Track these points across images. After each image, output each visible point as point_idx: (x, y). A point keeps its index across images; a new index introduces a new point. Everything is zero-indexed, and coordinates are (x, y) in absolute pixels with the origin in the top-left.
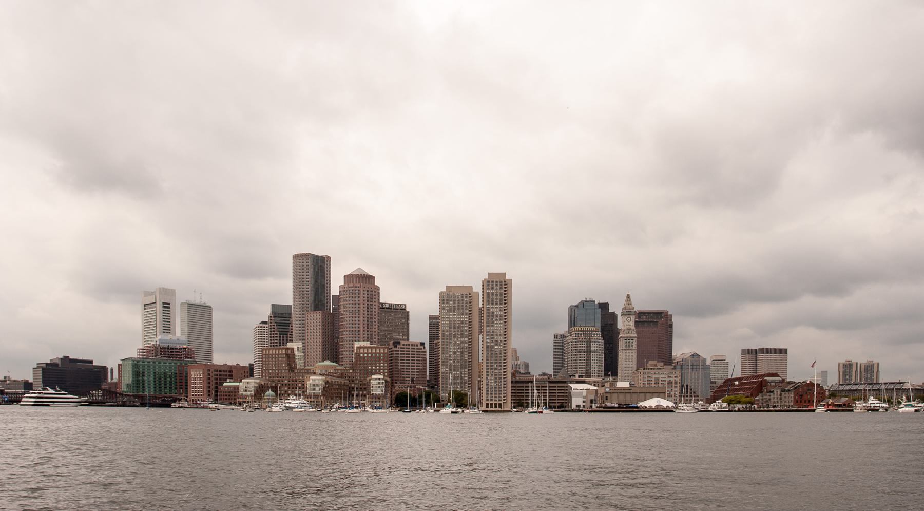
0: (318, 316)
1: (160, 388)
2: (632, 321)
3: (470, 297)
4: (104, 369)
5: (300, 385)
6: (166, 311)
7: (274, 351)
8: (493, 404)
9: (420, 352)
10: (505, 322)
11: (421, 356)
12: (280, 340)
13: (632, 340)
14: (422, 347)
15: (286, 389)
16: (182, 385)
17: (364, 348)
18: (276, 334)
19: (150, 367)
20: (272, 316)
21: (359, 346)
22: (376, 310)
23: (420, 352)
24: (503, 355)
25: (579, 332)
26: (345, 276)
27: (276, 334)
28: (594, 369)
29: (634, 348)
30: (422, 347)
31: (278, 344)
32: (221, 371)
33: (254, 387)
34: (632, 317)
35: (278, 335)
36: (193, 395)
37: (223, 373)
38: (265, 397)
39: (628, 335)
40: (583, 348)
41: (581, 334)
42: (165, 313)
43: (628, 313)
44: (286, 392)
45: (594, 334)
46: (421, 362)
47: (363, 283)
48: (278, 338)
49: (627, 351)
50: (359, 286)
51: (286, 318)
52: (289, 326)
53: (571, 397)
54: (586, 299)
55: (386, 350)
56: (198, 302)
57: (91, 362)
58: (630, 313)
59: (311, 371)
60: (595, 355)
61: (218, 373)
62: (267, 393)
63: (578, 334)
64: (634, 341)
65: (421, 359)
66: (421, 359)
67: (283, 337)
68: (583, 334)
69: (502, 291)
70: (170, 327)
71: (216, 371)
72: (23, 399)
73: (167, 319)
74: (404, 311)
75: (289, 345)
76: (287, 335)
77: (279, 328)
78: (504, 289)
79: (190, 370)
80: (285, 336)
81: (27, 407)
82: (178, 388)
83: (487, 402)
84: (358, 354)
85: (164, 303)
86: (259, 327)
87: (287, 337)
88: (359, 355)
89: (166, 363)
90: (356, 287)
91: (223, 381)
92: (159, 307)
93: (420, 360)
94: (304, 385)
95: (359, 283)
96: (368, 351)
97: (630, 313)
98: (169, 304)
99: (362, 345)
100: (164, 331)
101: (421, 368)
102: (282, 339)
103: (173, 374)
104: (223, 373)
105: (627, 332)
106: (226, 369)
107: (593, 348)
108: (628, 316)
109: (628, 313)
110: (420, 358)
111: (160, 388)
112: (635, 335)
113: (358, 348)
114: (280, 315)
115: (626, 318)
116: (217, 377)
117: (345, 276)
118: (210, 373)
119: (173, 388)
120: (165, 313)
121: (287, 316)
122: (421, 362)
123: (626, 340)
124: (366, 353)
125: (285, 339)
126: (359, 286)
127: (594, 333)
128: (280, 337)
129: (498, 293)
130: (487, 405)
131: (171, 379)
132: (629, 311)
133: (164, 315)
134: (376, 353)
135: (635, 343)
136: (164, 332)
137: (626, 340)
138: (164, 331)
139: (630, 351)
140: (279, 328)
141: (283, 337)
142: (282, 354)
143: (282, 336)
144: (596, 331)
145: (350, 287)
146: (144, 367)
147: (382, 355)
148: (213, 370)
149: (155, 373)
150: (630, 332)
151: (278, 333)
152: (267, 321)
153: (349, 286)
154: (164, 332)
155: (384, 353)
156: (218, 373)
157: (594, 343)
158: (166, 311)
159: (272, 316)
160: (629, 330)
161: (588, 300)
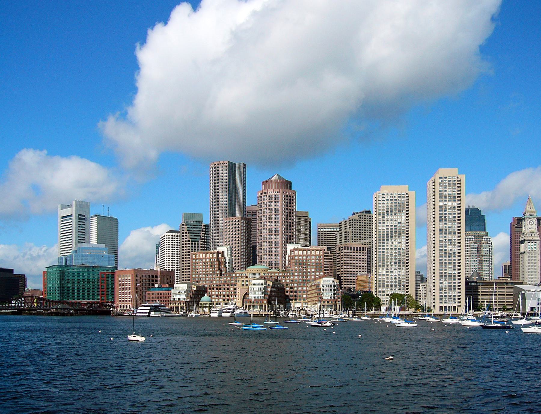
0: (237, 221)
2: (534, 225)
6: (81, 222)
11: (328, 260)
12: (192, 247)
13: (535, 243)
14: (329, 252)
15: (217, 293)
18: (189, 241)
20: (185, 224)
21: (293, 248)
22: (293, 218)
24: (457, 258)
25: (470, 237)
26: (116, 220)
27: (189, 241)
29: (537, 251)
30: (329, 252)
31: (190, 251)
32: (149, 276)
33: (59, 273)
34: (534, 221)
35: (190, 242)
38: (201, 302)
39: (531, 238)
40: (475, 252)
41: (472, 239)
42: (83, 225)
43: (530, 217)
44: (217, 296)
45: (485, 239)
46: (328, 266)
48: (190, 245)
49: (531, 254)
50: (279, 191)
51: (196, 225)
58: (532, 216)
61: (146, 278)
63: (470, 239)
65: (328, 263)
66: (328, 263)
67: (195, 244)
70: (84, 237)
71: (143, 276)
72: (149, 308)
73: (82, 230)
74: (306, 218)
75: (219, 249)
76: (198, 241)
79: (118, 276)
83: (441, 305)
84: (292, 258)
85: (80, 215)
86: (167, 236)
87: (198, 244)
89: (99, 270)
90: (276, 192)
92: (74, 220)
94: (235, 289)
95: (278, 188)
96: (303, 253)
97: (532, 216)
98: (84, 216)
99: (296, 248)
100: (79, 241)
101: (328, 271)
102: (194, 245)
103: (96, 280)
105: (530, 235)
106: (153, 274)
107: (484, 252)
108: (531, 219)
109: (530, 217)
110: (327, 262)
111: (93, 294)
112: (538, 238)
113: (292, 251)
117: (116, 220)
118: (139, 278)
119: (91, 288)
120: (83, 225)
122: (328, 266)
123: (529, 243)
124: (305, 256)
125: (197, 245)
126: (279, 191)
127: (485, 237)
128: (192, 244)
130: (441, 308)
131: (84, 283)
132: (531, 215)
133: (79, 226)
134: (311, 256)
136: (79, 242)
137: (529, 243)
138: (79, 241)
139: (534, 254)
141: (195, 244)
142: (213, 258)
144: (486, 236)
145: (269, 193)
146: (89, 274)
147: (313, 257)
148: (141, 276)
149: (84, 280)
152: (178, 230)
153: (269, 191)
154: (79, 242)
156: (146, 278)
157: (473, 247)
158: (81, 222)
160: (532, 233)
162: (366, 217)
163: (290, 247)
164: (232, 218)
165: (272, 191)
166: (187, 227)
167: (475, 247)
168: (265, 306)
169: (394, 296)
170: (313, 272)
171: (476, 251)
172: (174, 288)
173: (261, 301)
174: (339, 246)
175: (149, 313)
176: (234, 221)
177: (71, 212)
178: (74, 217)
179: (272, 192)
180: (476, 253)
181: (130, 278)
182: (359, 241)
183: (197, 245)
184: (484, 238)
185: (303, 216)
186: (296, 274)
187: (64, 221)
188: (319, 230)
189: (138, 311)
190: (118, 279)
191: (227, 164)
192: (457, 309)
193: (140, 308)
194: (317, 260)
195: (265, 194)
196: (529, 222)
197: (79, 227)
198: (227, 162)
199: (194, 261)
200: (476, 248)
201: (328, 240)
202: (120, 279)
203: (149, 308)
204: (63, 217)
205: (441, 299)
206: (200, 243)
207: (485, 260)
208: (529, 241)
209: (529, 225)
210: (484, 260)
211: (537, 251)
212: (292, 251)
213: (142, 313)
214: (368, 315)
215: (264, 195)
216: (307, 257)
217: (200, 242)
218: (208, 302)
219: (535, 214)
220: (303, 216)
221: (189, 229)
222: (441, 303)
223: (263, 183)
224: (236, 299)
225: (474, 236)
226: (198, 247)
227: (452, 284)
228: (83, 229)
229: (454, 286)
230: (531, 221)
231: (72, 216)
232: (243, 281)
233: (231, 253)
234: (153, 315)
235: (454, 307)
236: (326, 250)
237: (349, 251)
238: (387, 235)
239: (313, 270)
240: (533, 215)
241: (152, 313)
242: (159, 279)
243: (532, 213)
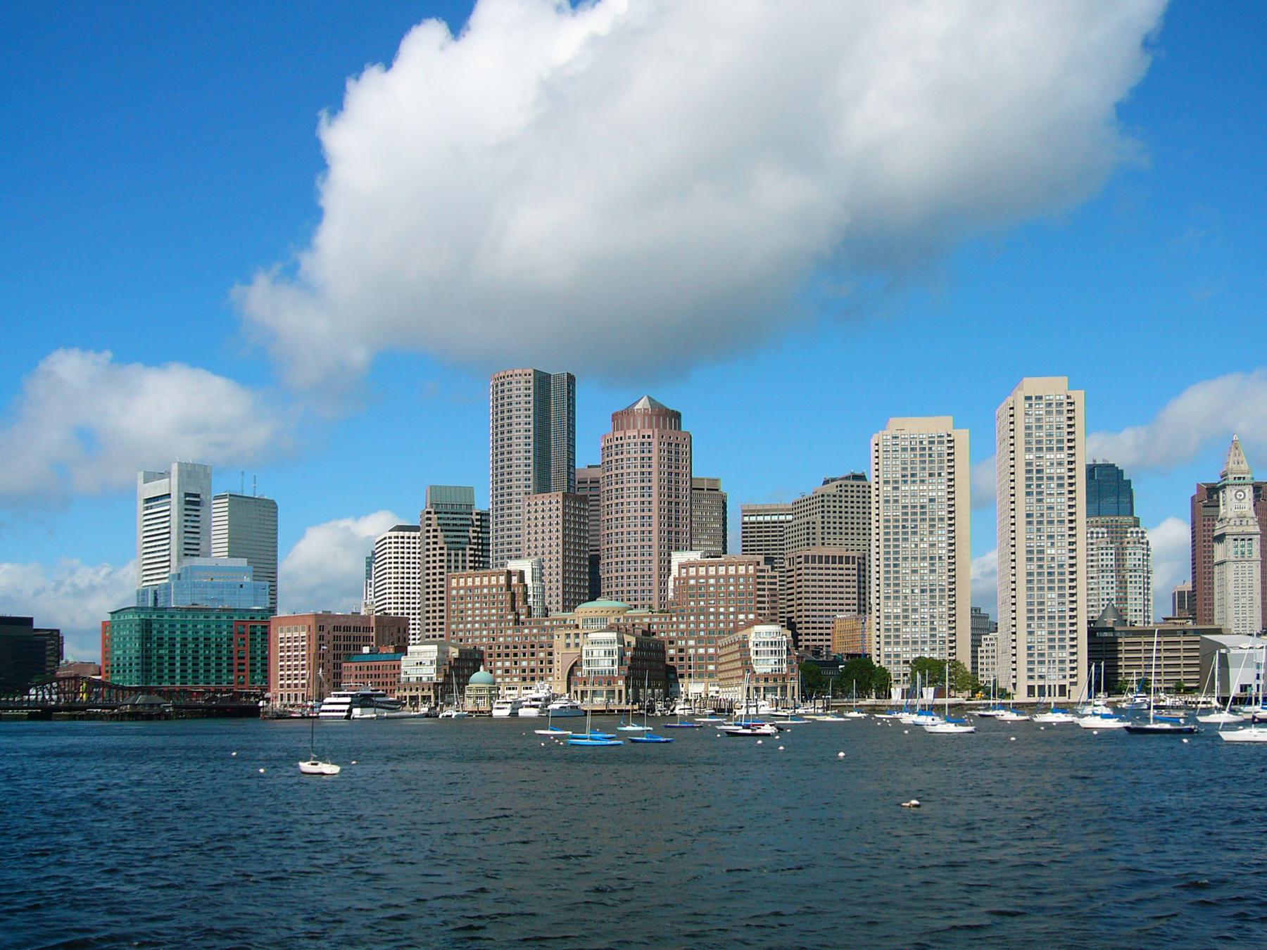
1: (219, 671)
2: (1247, 500)
3: (949, 441)
4: (54, 638)
5: (542, 655)
6: (191, 510)
7: (478, 580)
8: (1033, 687)
9: (764, 577)
10: (1071, 492)
11: (766, 587)
12: (449, 561)
13: (1250, 539)
14: (769, 567)
15: (507, 664)
16: (243, 664)
17: (691, 565)
18: (441, 548)
19: (209, 626)
20: (432, 510)
21: (684, 560)
23: (764, 577)
25: (1098, 529)
26: (272, 505)
27: (441, 548)
28: (1134, 608)
29: (1254, 557)
30: (769, 567)
32: (347, 629)
34: (1246, 491)
35: (445, 551)
36: (282, 686)
37: (352, 634)
38: (470, 686)
39: (1240, 529)
40: (1109, 563)
41: (1103, 533)
43: (1237, 481)
45: (1132, 532)
47: (658, 426)
49: (1240, 566)
50: (651, 434)
52: (468, 531)
53: (1228, 667)
54: (1094, 461)
55: (751, 568)
56: (248, 493)
57: (29, 621)
59: (568, 622)
60: (1135, 576)
61: (341, 633)
62: (475, 676)
63: (1098, 533)
64: (1254, 542)
65: (766, 593)
66: (766, 593)
67: (457, 555)
68: (1108, 533)
69: (1064, 418)
70: (198, 544)
71: (336, 628)
72: (348, 700)
74: (715, 492)
77: (447, 537)
78: (1066, 415)
80: (460, 552)
81: (687, 729)
82: (236, 670)
83: (1031, 683)
85: (187, 495)
87: (464, 555)
88: (688, 582)
90: (644, 437)
91: (352, 652)
93: (763, 596)
94: (550, 654)
95: (650, 427)
98: (197, 496)
101: (766, 612)
104: (352, 634)
105: (1238, 523)
106: (358, 624)
108: (1240, 488)
109: (1237, 481)
110: (764, 590)
111: (219, 671)
112: (1257, 529)
113: (681, 566)
114: (449, 509)
115: (1234, 492)
116: (338, 643)
118: (325, 633)
121: (463, 509)
122: (766, 599)
123: (1235, 540)
124: (712, 577)
125: (460, 558)
126: (651, 434)
127: (1132, 529)
128: (449, 555)
129: (899, 448)
130: (1031, 690)
132: (1239, 478)
134: (727, 577)
135: (1256, 546)
136: (186, 555)
137: (1235, 540)
139: (1247, 564)
140: (447, 537)
141: (457, 555)
143: (453, 552)
145: (629, 438)
147: (732, 580)
148: (330, 628)
149: (197, 639)
150: (1244, 523)
151: (445, 546)
153: (628, 434)
154: (186, 555)
155: (746, 576)
156: (341, 633)
158: (191, 510)
159: (432, 510)
160: (1242, 517)
161: (1099, 462)
162: (855, 489)
163: (678, 558)
164: (541, 495)
165: (636, 434)
166: (438, 518)
167: (1110, 552)
168: (620, 692)
169: (920, 665)
170: (732, 613)
171: (1111, 560)
172: (406, 655)
173: (610, 680)
174: (793, 555)
175: (350, 711)
176: (547, 502)
177: (168, 488)
178: (174, 499)
179: (634, 437)
180: (1111, 565)
181: (304, 634)
182: (838, 541)
183: (460, 558)
184: (1129, 530)
185: (708, 489)
186: (692, 618)
187: (151, 507)
188: (746, 519)
189: (324, 707)
190: (276, 636)
191: (530, 375)
192: (1069, 691)
193: (327, 700)
194: (741, 587)
195: (620, 442)
196: (1236, 495)
197: (186, 521)
198: (531, 371)
199: (454, 592)
200: (1111, 554)
201: (766, 536)
202: (281, 635)
203: (348, 700)
204: (148, 500)
205: (1031, 670)
206: (468, 552)
207: (1133, 579)
208: (1235, 537)
209: (1234, 500)
210: (1129, 580)
211: (1254, 557)
212: (681, 566)
213: (333, 711)
214: (860, 709)
215: (617, 443)
216: (717, 581)
217: (468, 550)
218: (487, 683)
219: (1249, 476)
220: (708, 489)
221: (441, 522)
222: (1031, 678)
223: (615, 417)
224: (552, 676)
225: (1107, 527)
226: (464, 561)
227: (1057, 636)
228: (196, 525)
229: (1062, 640)
230: (1239, 491)
231: (170, 497)
232: (568, 636)
233: (539, 574)
234: (358, 716)
235: (1062, 688)
236: (762, 563)
237: (817, 565)
238: (904, 527)
239: (732, 609)
240: (1244, 478)
241: (357, 712)
242: (373, 634)
243: (1242, 473)
